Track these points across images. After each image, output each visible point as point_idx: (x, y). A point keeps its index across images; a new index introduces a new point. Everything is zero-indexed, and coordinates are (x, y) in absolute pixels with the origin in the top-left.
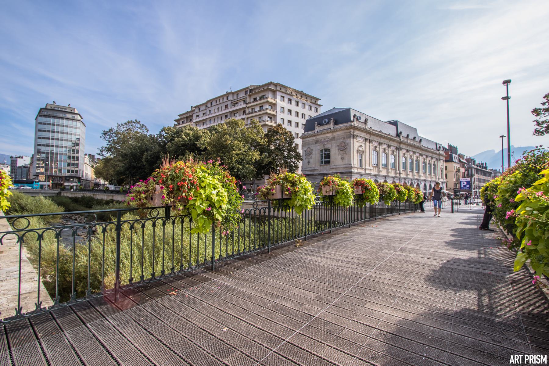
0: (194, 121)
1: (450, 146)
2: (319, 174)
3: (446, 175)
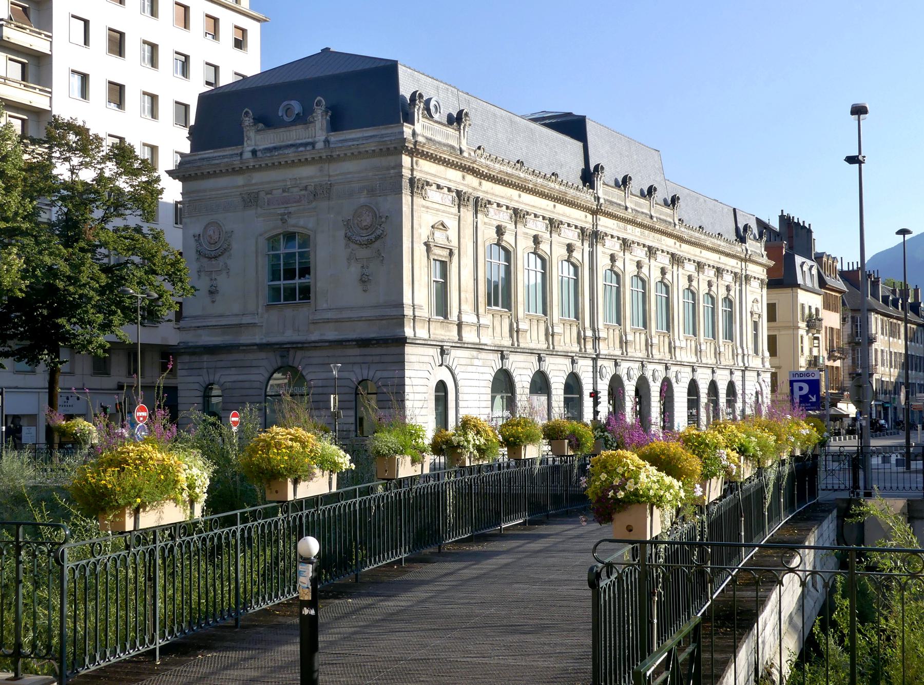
1: (785, 220)
2: (262, 347)
3: (772, 342)
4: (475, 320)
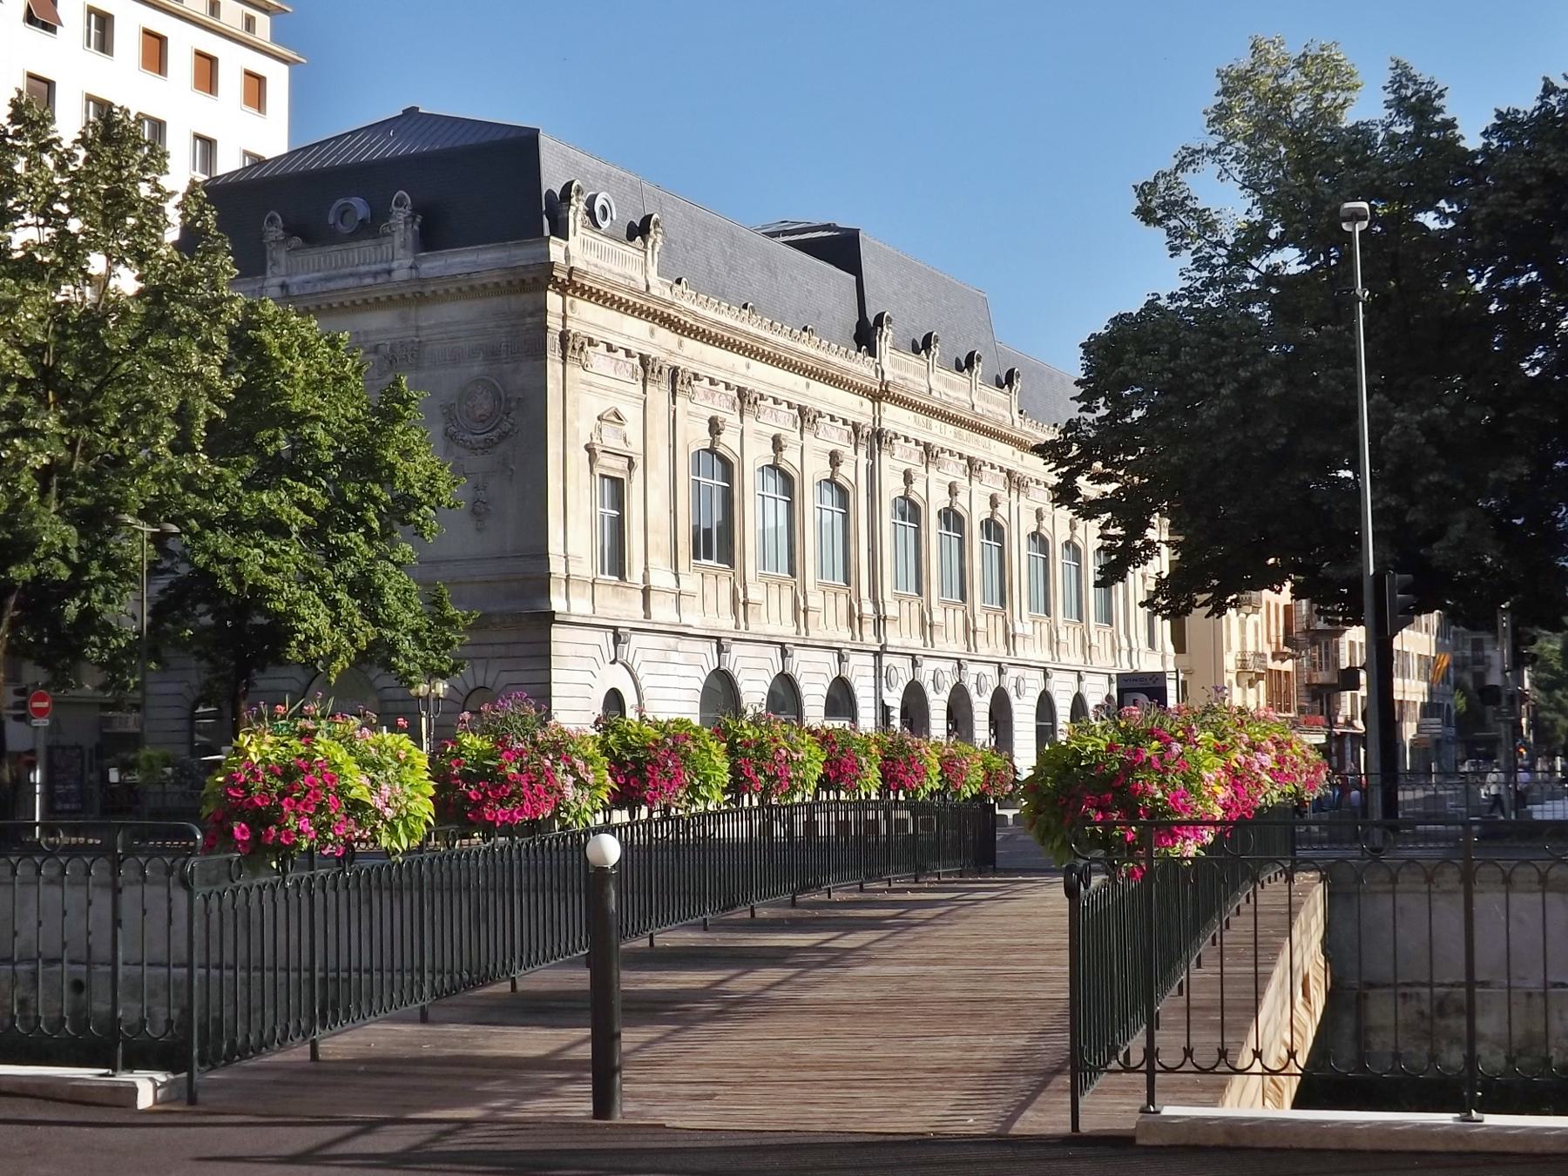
4: (672, 583)
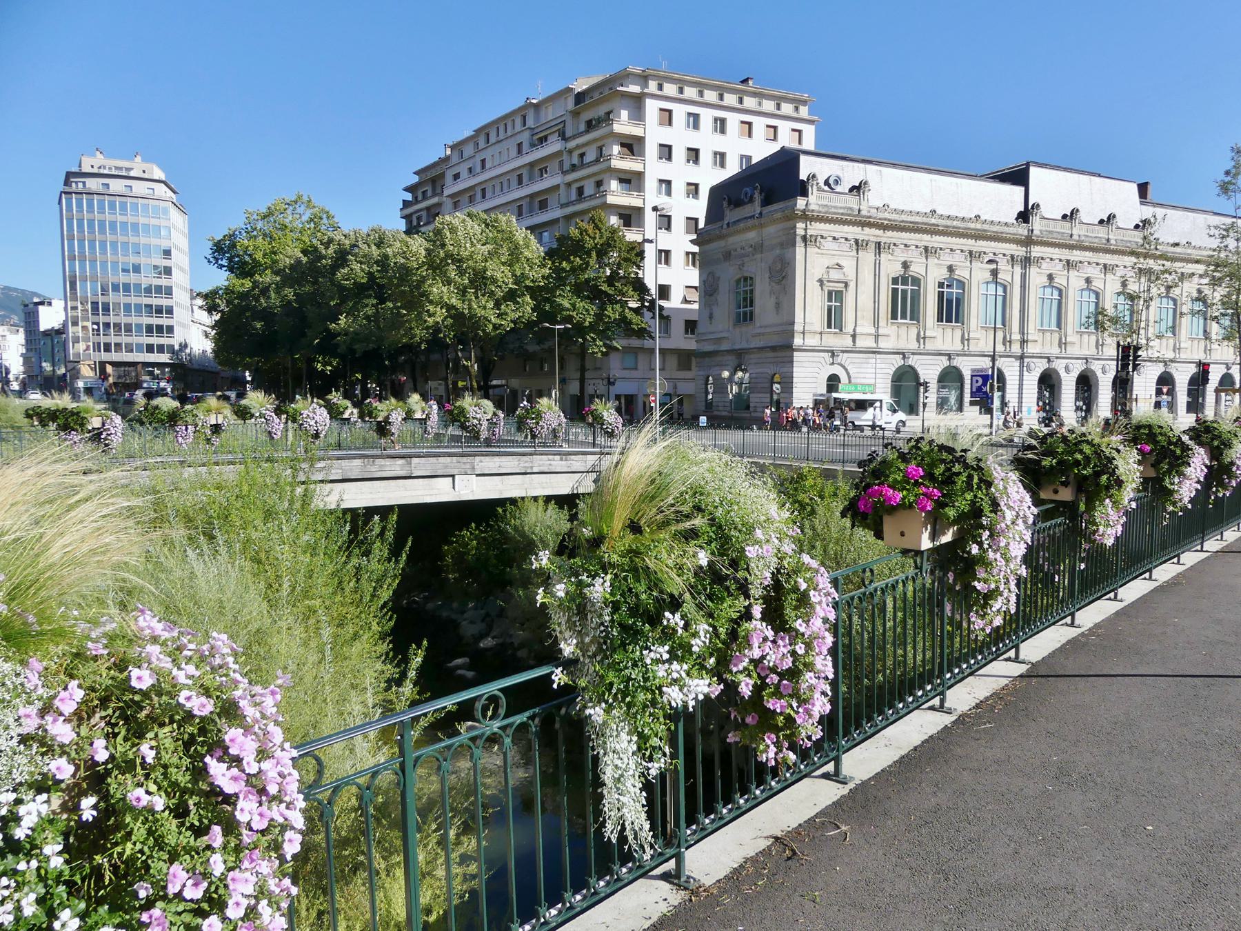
0: (447, 192)
4: (872, 330)
